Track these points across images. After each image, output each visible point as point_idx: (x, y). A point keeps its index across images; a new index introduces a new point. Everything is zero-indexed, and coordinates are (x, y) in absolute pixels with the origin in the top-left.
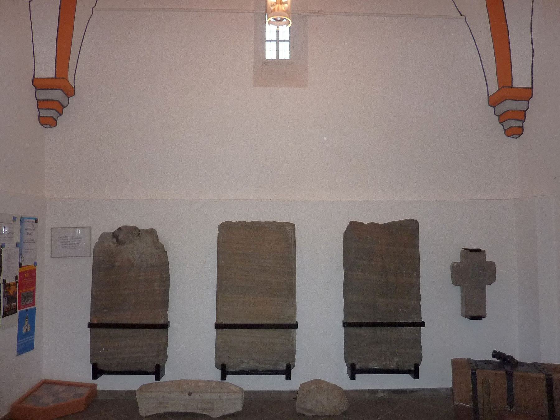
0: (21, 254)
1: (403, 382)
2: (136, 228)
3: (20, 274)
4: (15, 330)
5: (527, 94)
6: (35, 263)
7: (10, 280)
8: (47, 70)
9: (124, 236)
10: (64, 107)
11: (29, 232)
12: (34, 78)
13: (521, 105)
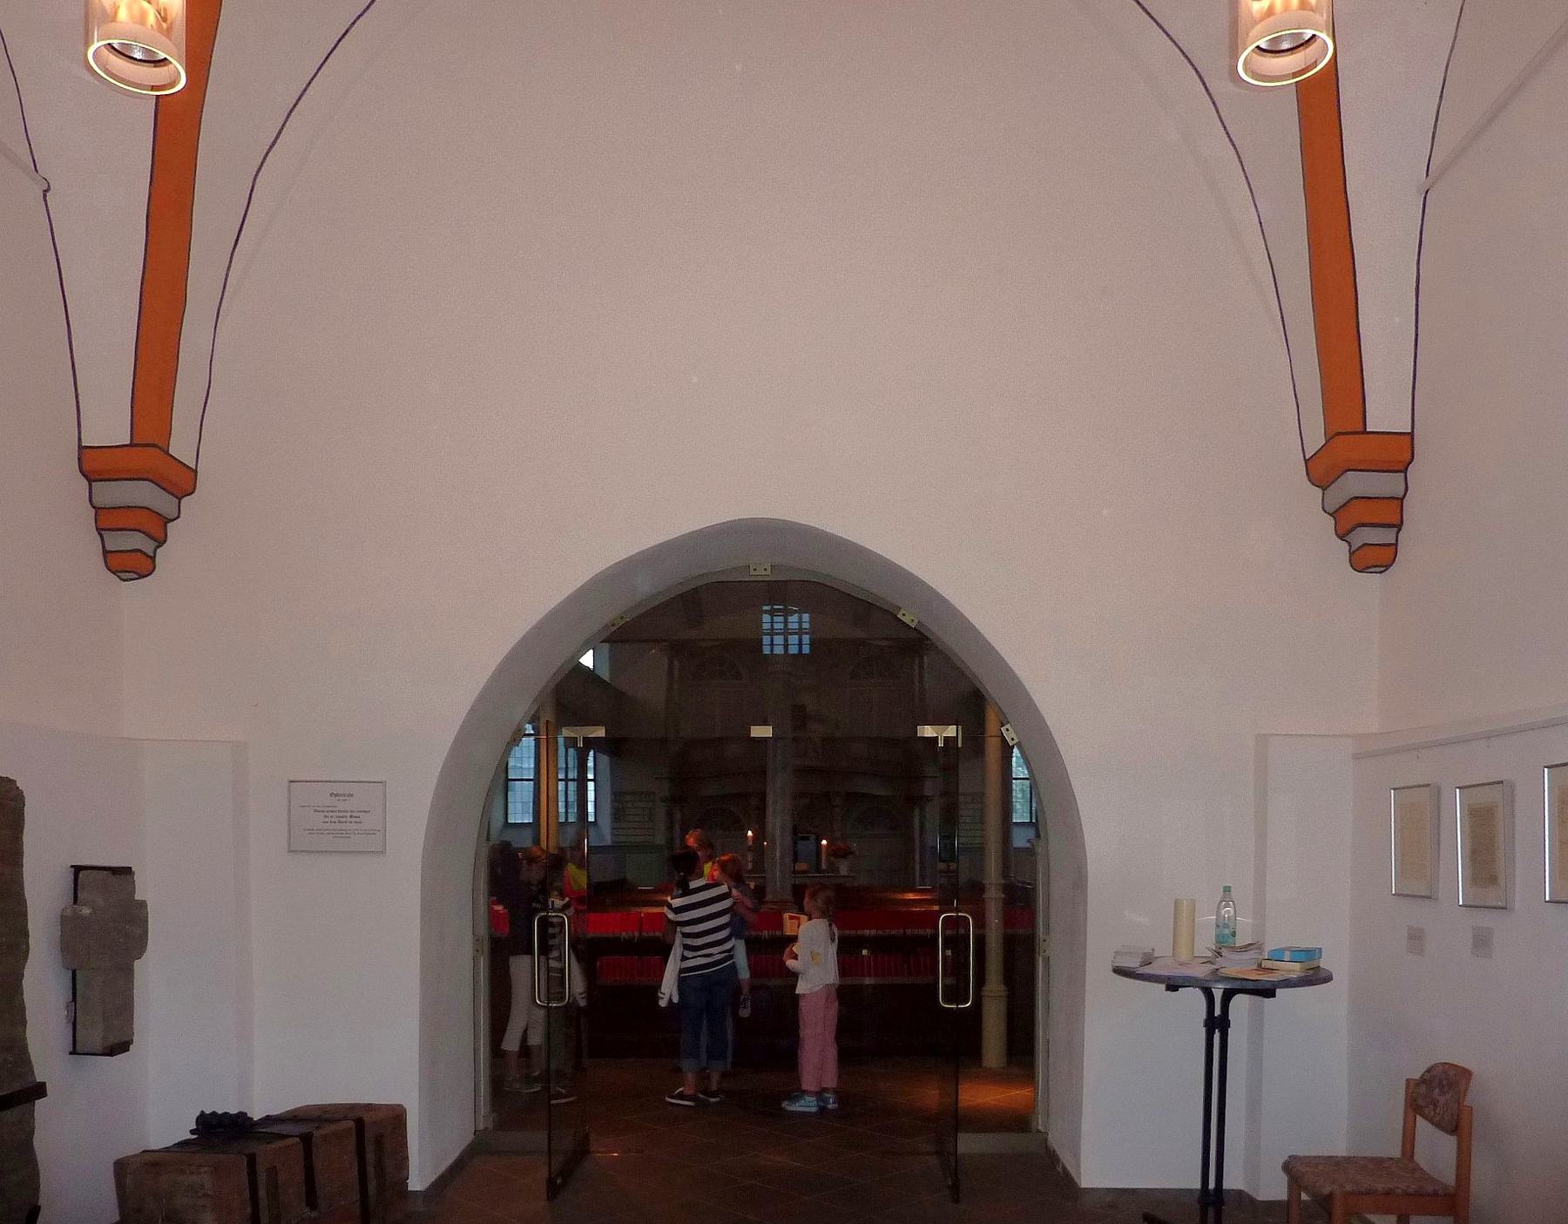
5: (1399, 453)
8: (110, 425)
10: (1402, 499)
12: (81, 448)
13: (1385, 484)
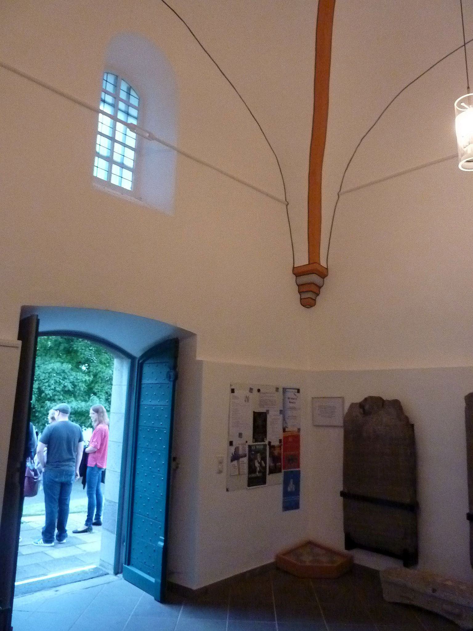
0: (284, 419)
1: (268, 472)
2: (380, 399)
3: (284, 438)
4: (279, 489)
6: (299, 430)
7: (275, 443)
9: (371, 406)
11: (292, 401)
12: (294, 267)
